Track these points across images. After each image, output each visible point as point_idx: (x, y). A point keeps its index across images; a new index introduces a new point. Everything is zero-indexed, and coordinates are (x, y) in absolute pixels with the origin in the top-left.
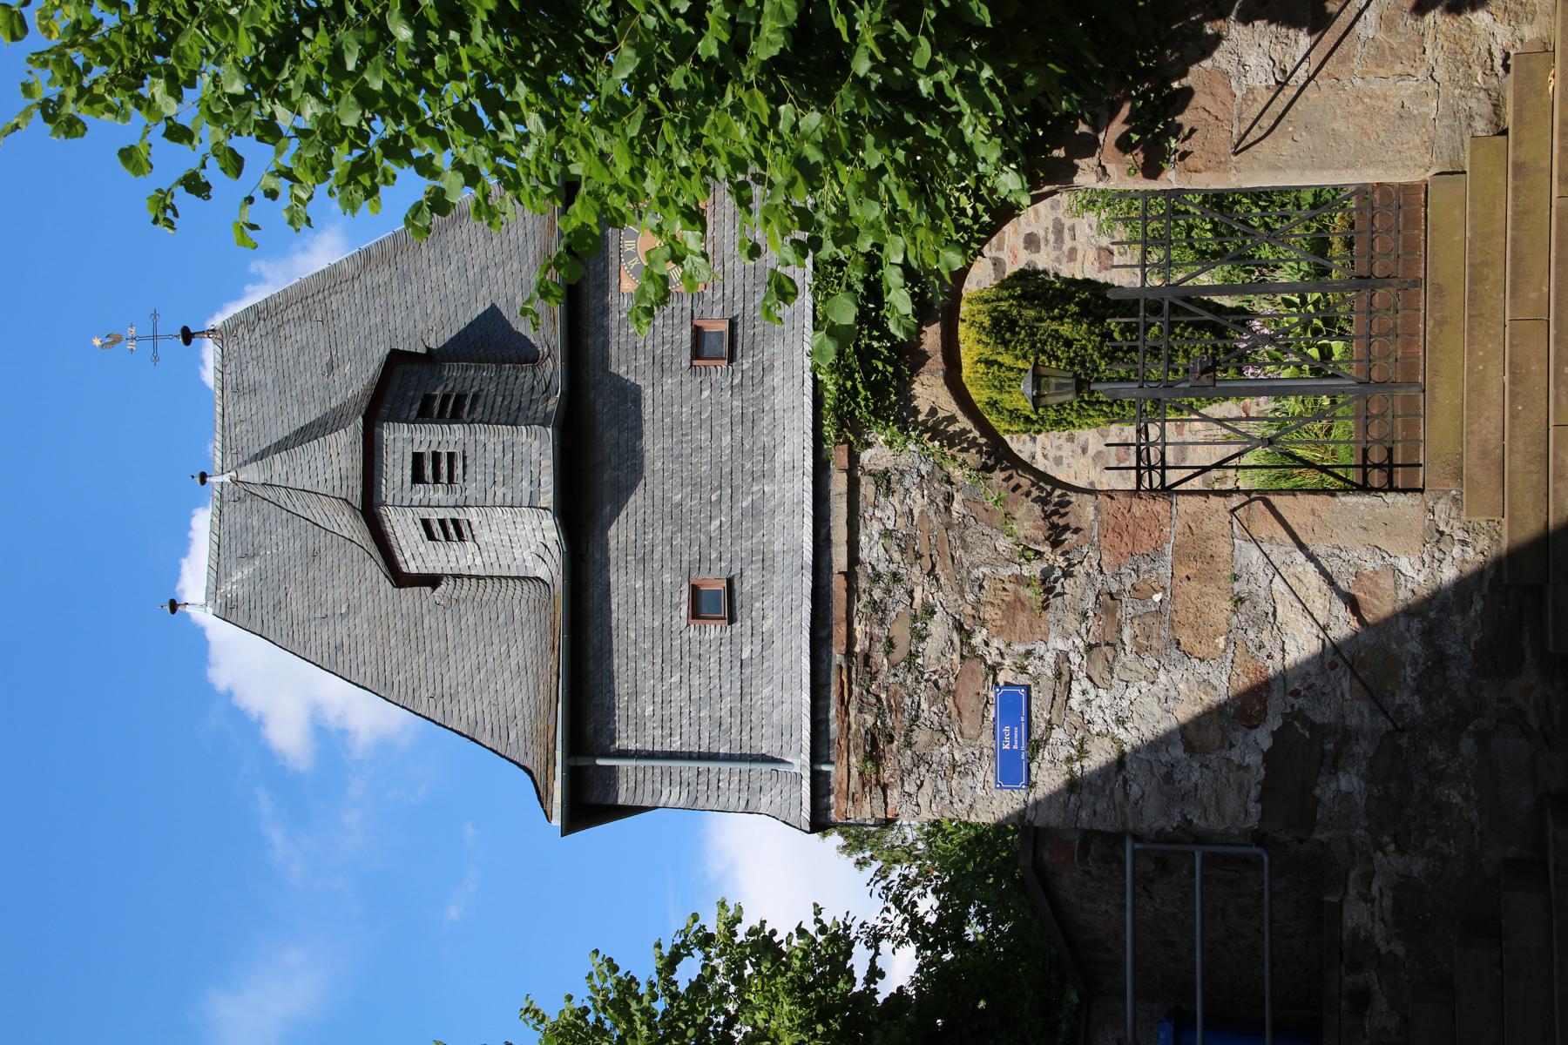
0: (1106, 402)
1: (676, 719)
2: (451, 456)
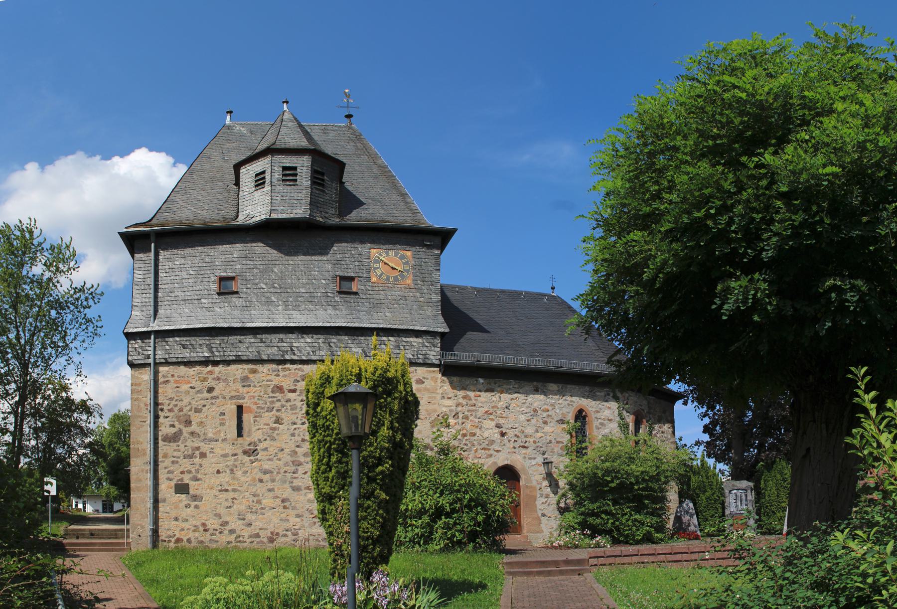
0: (330, 461)
1: (173, 274)
2: (296, 180)
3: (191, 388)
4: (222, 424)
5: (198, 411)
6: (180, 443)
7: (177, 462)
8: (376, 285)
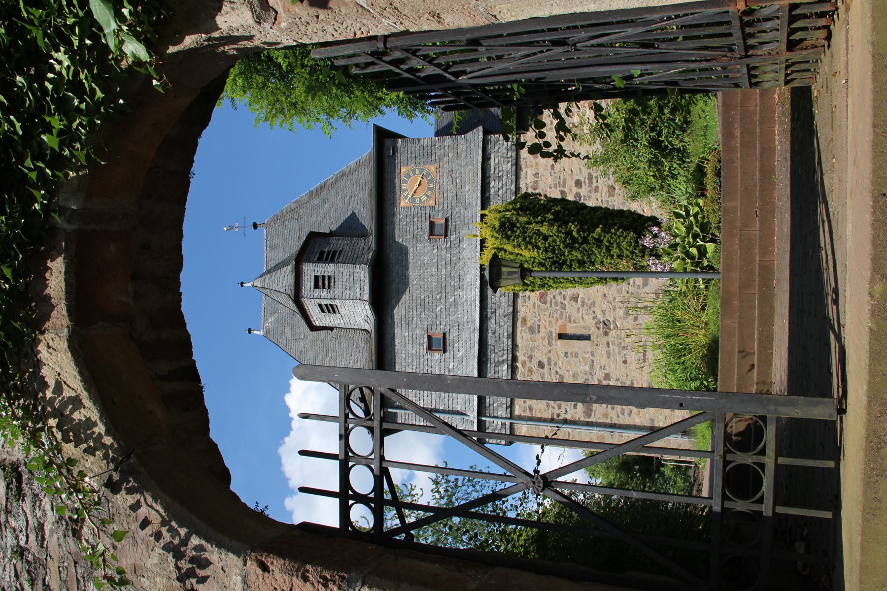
2: (329, 277)
4: (576, 355)
8: (437, 200)
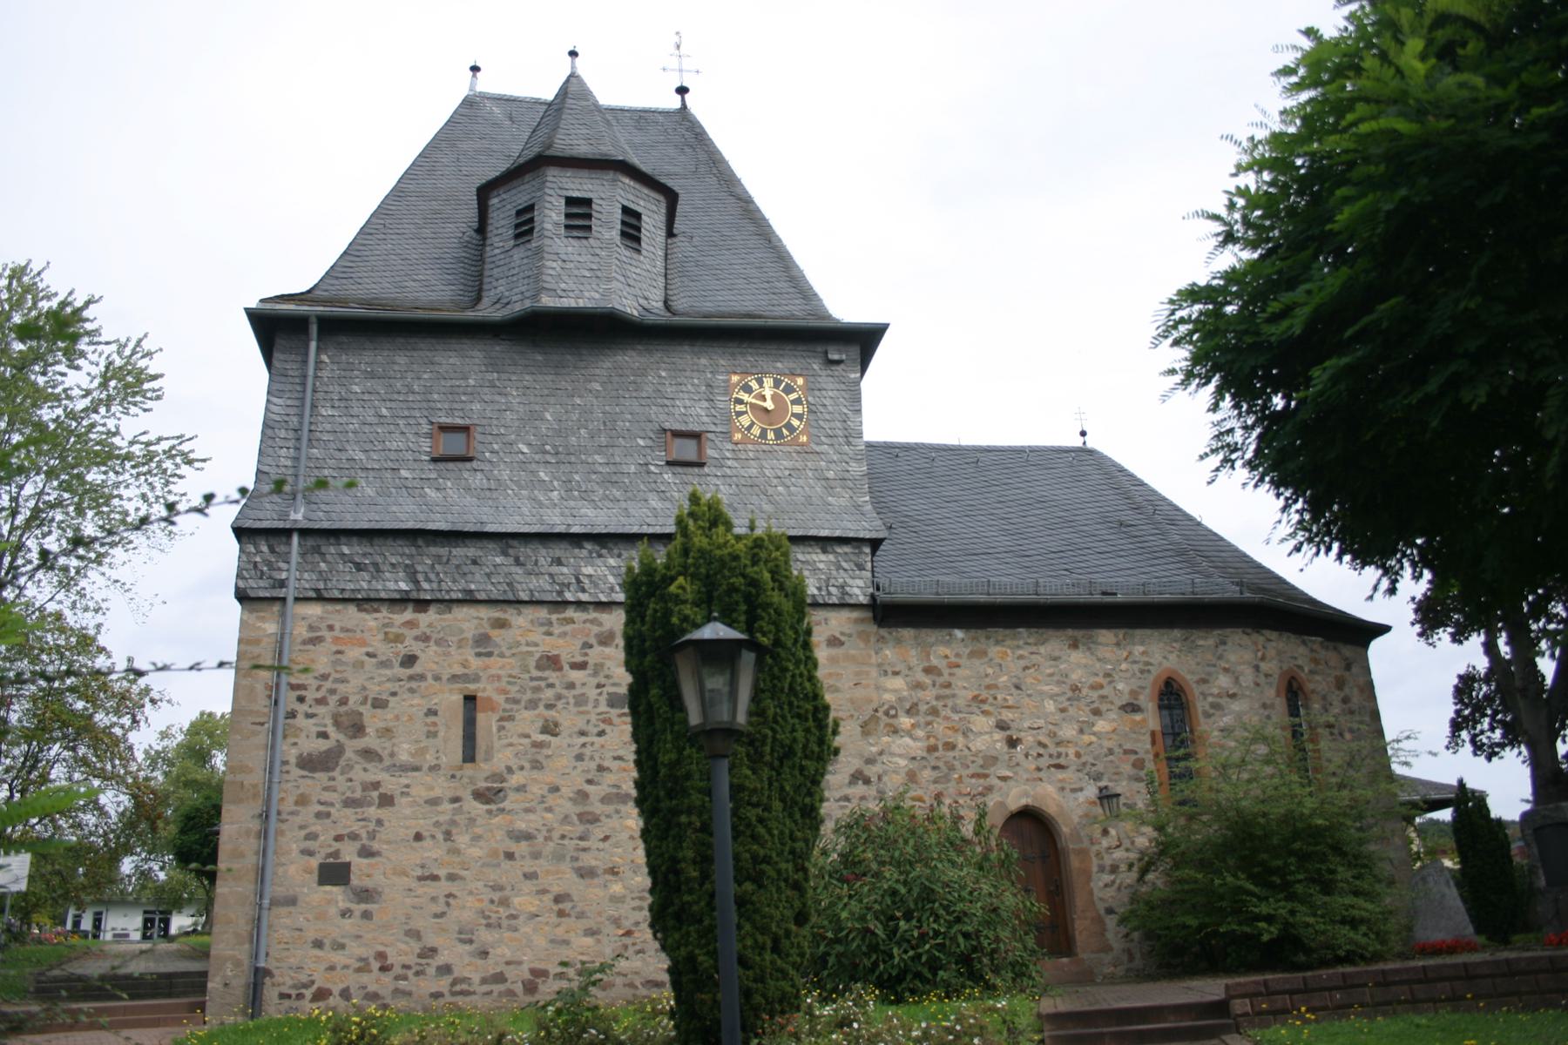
3: (368, 654)
4: (432, 735)
5: (379, 704)
6: (336, 774)
7: (328, 815)
